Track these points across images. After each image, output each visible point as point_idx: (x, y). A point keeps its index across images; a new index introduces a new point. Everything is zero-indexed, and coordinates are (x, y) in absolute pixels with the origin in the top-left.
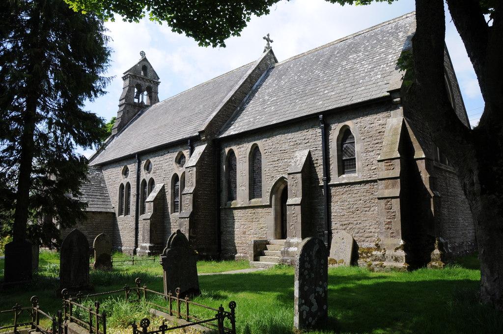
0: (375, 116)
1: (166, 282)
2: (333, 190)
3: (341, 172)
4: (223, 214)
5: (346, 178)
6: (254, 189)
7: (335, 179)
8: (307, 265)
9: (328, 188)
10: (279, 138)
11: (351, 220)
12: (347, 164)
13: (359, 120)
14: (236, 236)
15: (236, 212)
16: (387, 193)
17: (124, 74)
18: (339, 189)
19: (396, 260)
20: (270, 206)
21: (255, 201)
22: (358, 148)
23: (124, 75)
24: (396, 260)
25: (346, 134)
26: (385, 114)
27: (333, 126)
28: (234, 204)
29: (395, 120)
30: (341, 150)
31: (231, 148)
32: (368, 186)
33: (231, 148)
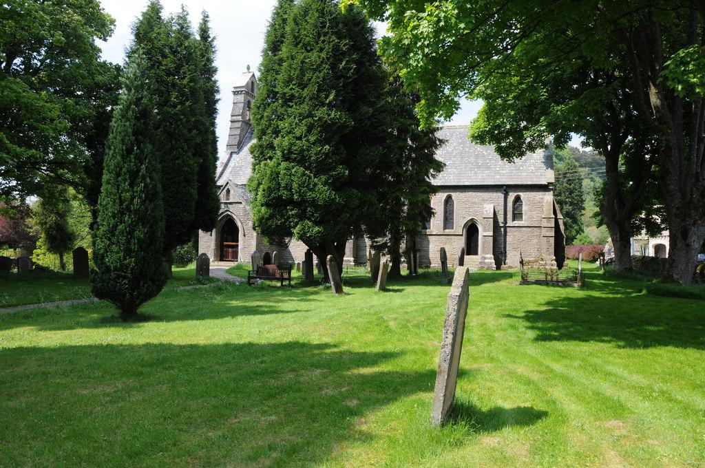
0: (537, 193)
1: (79, 332)
2: (508, 229)
3: (514, 220)
4: (418, 240)
5: (516, 223)
6: (448, 220)
7: (510, 223)
8: (47, 355)
9: (505, 228)
10: (470, 194)
11: (519, 246)
12: (517, 215)
13: (527, 193)
14: (430, 254)
15: (431, 238)
16: (547, 234)
17: (234, 88)
18: (512, 229)
19: (552, 265)
20: (462, 235)
21: (447, 231)
22: (524, 208)
23: (233, 90)
24: (552, 265)
25: (518, 199)
26: (543, 193)
27: (510, 194)
28: (428, 232)
29: (549, 197)
30: (514, 209)
31: (519, 193)
32: (530, 229)
33: (519, 193)
